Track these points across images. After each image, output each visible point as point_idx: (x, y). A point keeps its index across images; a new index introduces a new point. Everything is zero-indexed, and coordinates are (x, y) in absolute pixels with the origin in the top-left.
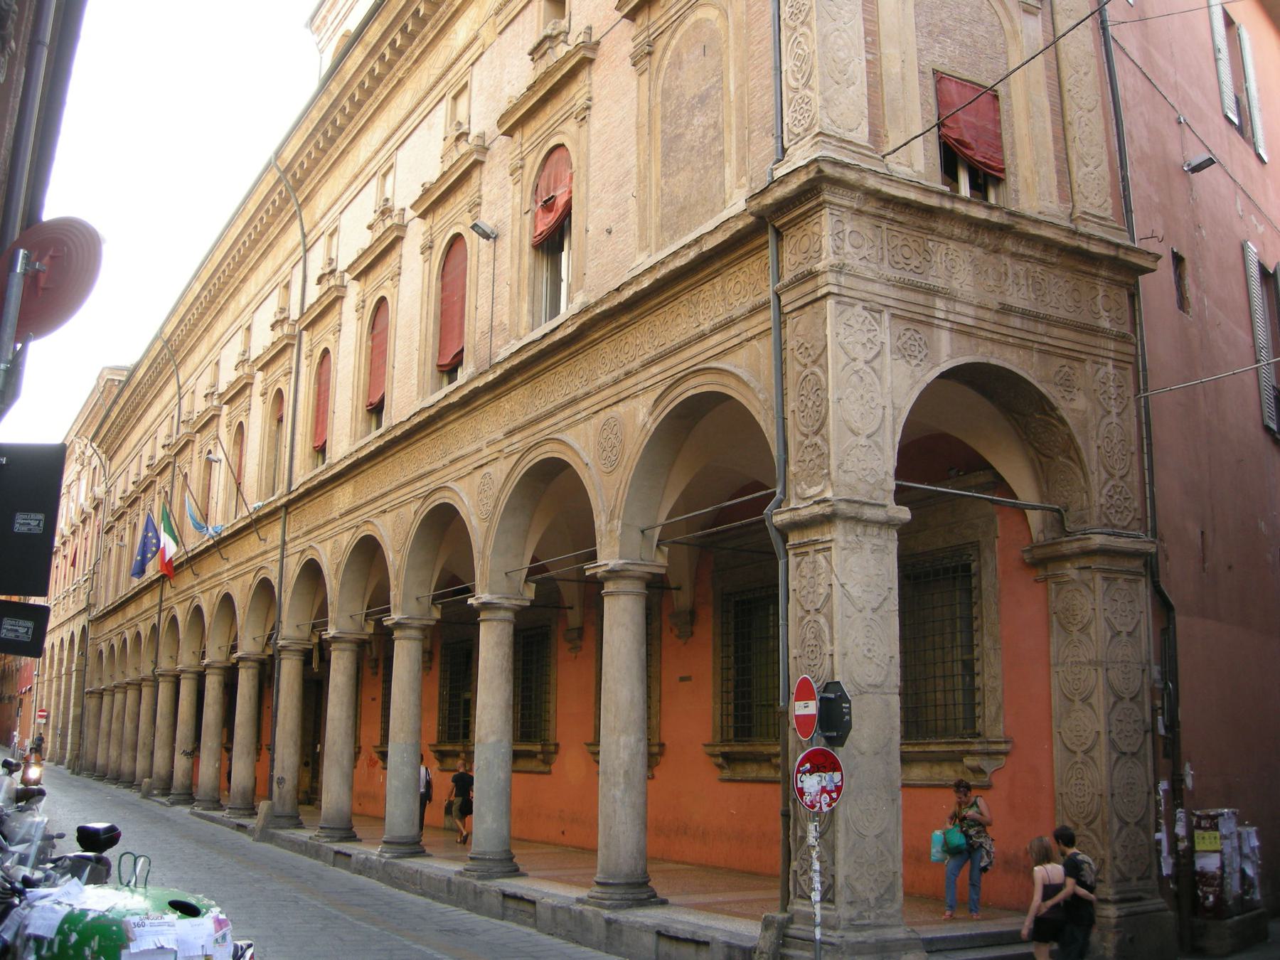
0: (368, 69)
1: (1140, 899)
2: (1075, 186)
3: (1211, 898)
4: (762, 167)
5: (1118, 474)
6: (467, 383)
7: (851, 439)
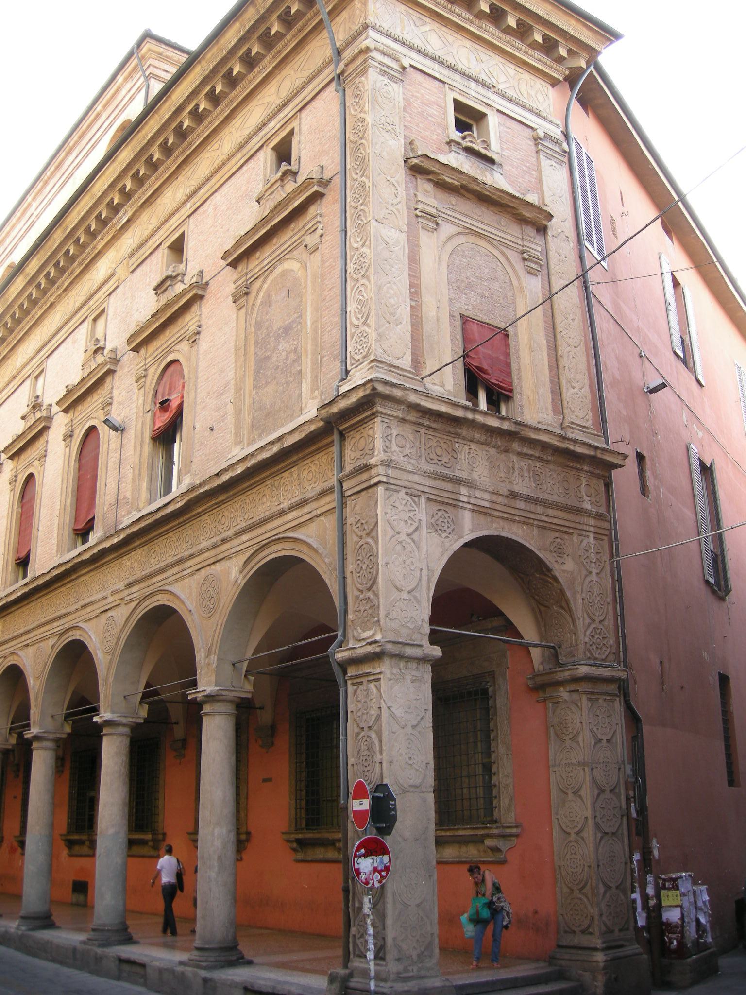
0: (27, 294)
1: (621, 946)
2: (565, 403)
3: (675, 943)
4: (330, 384)
5: (598, 619)
6: (96, 545)
7: (395, 595)
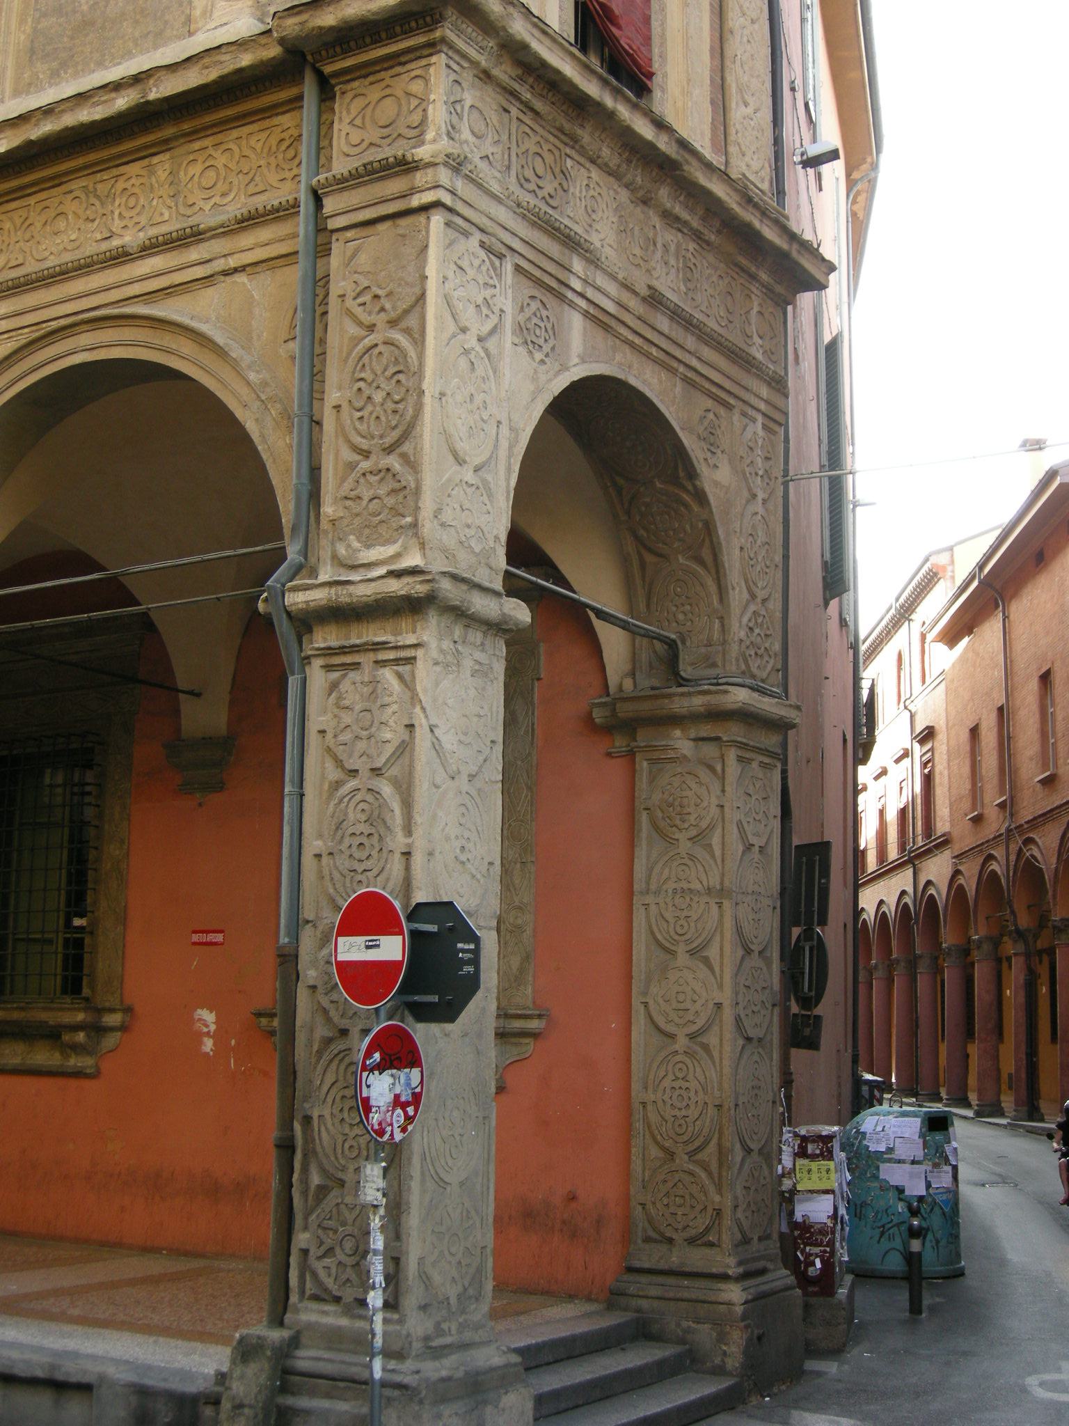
1: (763, 1272)
2: (732, 131)
5: (761, 594)
7: (452, 469)
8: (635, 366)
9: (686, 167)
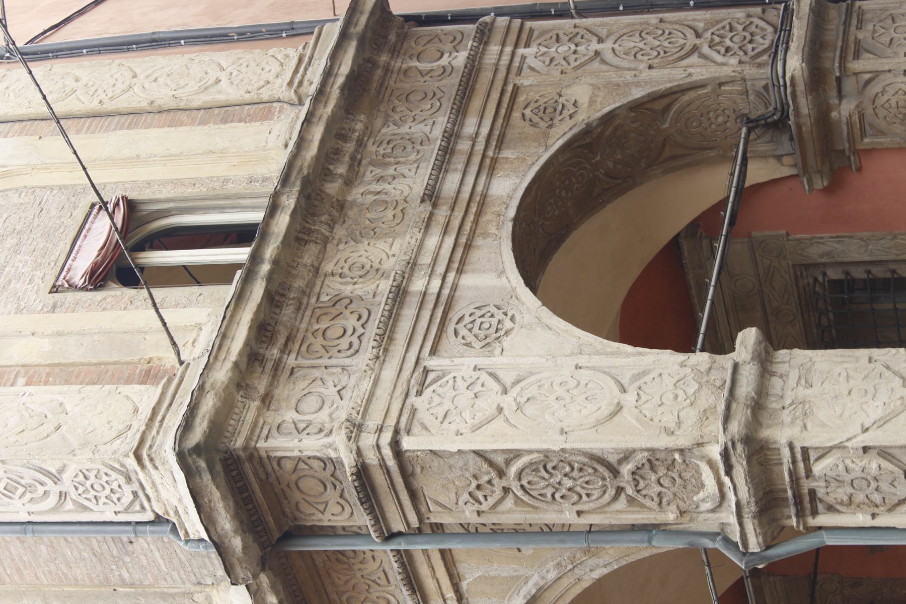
2: (248, 98)
5: (692, 40)
7: (628, 416)
8: (497, 209)
9: (305, 172)
